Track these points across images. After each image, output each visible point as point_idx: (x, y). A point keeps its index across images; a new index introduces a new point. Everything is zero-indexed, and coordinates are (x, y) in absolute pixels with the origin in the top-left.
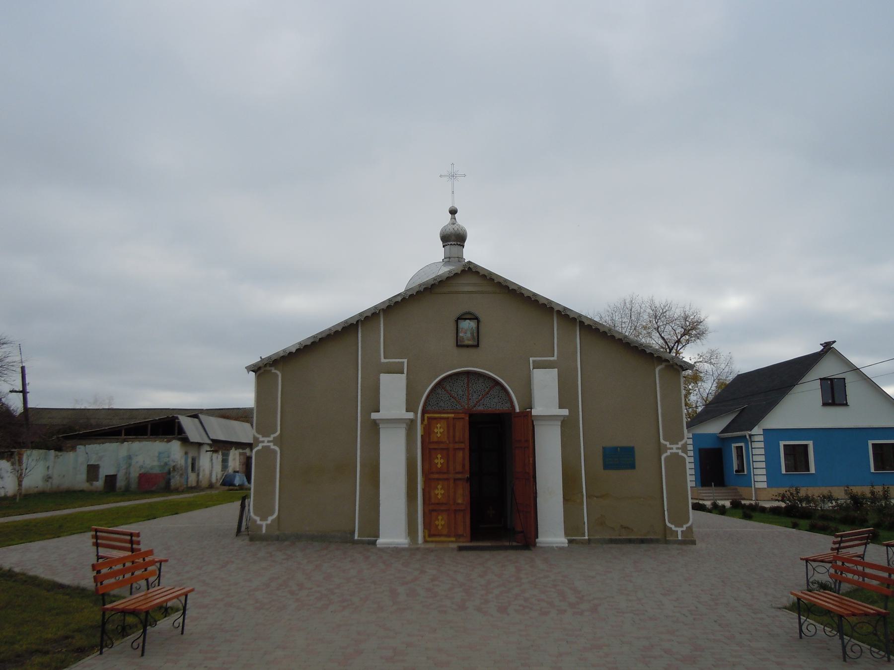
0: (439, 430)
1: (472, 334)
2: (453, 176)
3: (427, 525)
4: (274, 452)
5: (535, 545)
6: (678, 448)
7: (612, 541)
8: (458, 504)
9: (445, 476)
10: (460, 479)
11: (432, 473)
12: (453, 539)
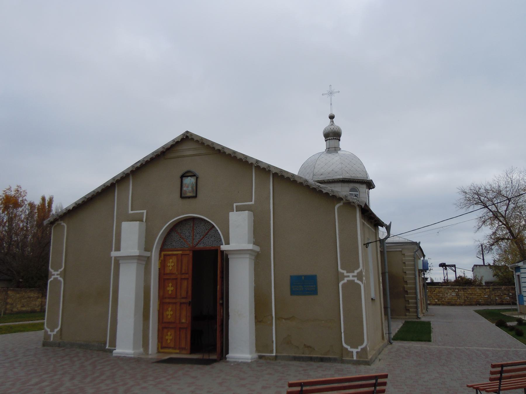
0: (171, 264)
1: (192, 187)
2: (331, 93)
3: (161, 338)
4: (60, 281)
5: (226, 358)
6: (353, 276)
7: (295, 359)
8: (183, 323)
9: (174, 301)
10: (184, 303)
11: (165, 298)
12: (178, 351)
